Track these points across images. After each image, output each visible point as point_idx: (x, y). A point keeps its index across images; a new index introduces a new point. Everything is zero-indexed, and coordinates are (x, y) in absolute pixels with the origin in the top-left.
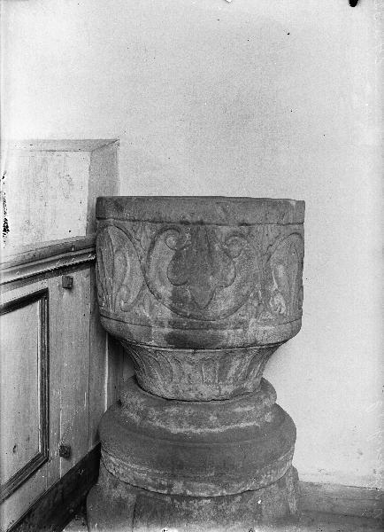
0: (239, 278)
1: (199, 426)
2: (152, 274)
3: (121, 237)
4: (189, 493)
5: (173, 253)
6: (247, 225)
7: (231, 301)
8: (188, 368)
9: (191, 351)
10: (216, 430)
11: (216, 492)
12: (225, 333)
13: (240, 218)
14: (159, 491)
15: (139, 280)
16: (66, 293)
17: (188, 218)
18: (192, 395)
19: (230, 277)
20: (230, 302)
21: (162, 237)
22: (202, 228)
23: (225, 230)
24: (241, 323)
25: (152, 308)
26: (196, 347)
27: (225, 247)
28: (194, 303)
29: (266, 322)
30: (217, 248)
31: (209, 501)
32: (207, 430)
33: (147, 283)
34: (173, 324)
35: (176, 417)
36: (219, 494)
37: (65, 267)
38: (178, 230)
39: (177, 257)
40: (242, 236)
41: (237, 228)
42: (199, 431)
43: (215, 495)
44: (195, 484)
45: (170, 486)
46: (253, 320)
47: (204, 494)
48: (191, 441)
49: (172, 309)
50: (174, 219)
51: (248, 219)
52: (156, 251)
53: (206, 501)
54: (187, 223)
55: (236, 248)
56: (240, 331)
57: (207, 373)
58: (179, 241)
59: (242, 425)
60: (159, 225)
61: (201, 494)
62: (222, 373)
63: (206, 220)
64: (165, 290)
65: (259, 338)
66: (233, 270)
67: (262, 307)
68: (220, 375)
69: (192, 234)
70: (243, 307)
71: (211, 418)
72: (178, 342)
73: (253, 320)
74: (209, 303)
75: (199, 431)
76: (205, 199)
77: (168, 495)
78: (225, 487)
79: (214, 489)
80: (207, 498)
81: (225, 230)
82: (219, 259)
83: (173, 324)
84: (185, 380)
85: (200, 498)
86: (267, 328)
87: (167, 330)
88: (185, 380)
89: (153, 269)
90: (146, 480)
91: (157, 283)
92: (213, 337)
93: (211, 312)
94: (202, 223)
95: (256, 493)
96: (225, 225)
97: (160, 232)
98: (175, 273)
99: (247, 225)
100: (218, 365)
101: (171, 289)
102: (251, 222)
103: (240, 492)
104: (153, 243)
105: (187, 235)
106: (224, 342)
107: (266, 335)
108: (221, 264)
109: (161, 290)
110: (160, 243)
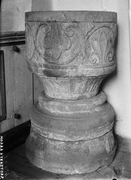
0: (72, 47)
1: (62, 110)
2: (37, 44)
3: (28, 29)
4: (55, 138)
5: (44, 35)
6: (76, 22)
7: (69, 57)
8: (57, 86)
9: (55, 78)
10: (69, 113)
11: (66, 139)
12: (67, 71)
13: (73, 19)
14: (44, 136)
15: (33, 47)
16: (16, 54)
17: (50, 20)
18: (60, 97)
19: (69, 46)
20: (69, 57)
21: (40, 28)
22: (56, 24)
23: (66, 25)
24: (74, 66)
25: (38, 59)
26: (57, 76)
27: (66, 32)
28: (53, 58)
29: (87, 67)
30: (62, 33)
31: (64, 142)
32: (65, 112)
33: (36, 49)
34: (45, 66)
35: (53, 106)
36: (68, 140)
37: (14, 42)
38: (46, 25)
39: (46, 37)
40: (74, 27)
41: (72, 24)
42: (62, 112)
43: (66, 140)
44: (57, 135)
45: (48, 135)
46: (81, 65)
47: (62, 139)
48: (57, 117)
49: (45, 59)
50: (45, 20)
51: (77, 20)
52: (38, 35)
53: (62, 142)
54: (49, 22)
55: (71, 33)
56: (74, 70)
57: (63, 88)
58: (47, 30)
59: (82, 112)
60: (39, 23)
61: (60, 139)
62: (72, 88)
63: (57, 20)
64: (42, 51)
65: (85, 74)
66: (70, 43)
67: (85, 60)
68: (71, 89)
69: (51, 26)
70: (75, 59)
71: (66, 107)
72: (48, 74)
73: (81, 65)
74: (60, 57)
75: (62, 112)
76: (69, 12)
77: (47, 138)
78: (70, 137)
79: (66, 138)
80: (63, 141)
81: (66, 25)
82: (63, 38)
83: (45, 66)
84: (57, 90)
85: (59, 141)
86: (88, 69)
87: (44, 69)
88: (57, 90)
89: (37, 41)
90: (40, 131)
91: (39, 48)
92: (62, 72)
93: (60, 61)
94: (55, 21)
95: (86, 141)
96: (66, 22)
97: (40, 26)
98: (46, 44)
99: (76, 22)
100: (69, 85)
101: (44, 51)
102: (78, 21)
103: (78, 140)
104: (37, 31)
105: (50, 27)
106: (67, 75)
107: (88, 72)
108: (64, 40)
109: (41, 51)
110: (40, 31)
